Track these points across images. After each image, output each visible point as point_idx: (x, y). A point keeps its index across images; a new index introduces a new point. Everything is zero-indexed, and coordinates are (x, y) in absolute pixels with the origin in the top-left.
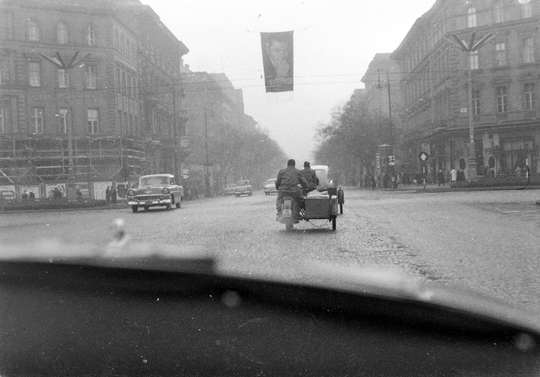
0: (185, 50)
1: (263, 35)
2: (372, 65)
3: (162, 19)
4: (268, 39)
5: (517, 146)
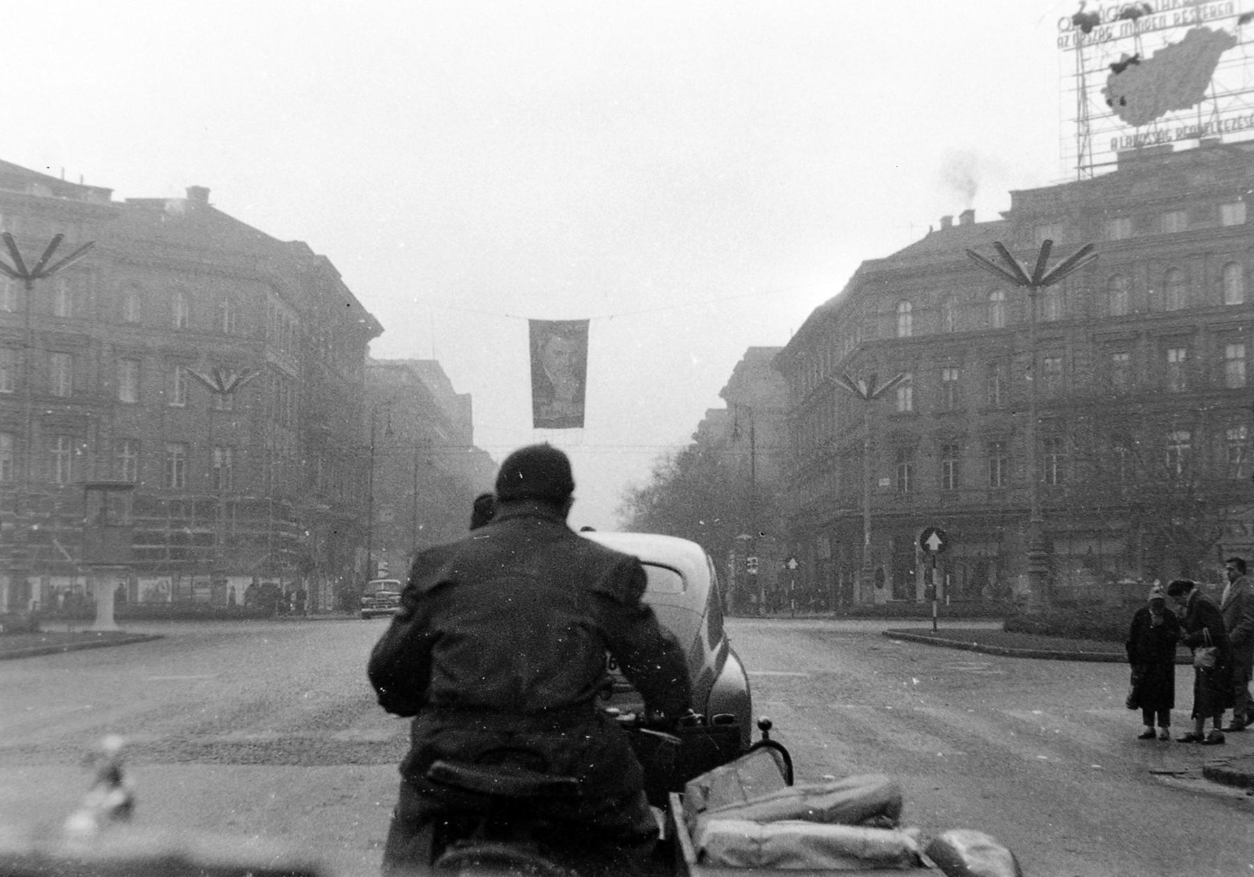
0: (377, 330)
1: (533, 324)
2: (741, 369)
3: (346, 279)
4: (542, 333)
5: (973, 551)
